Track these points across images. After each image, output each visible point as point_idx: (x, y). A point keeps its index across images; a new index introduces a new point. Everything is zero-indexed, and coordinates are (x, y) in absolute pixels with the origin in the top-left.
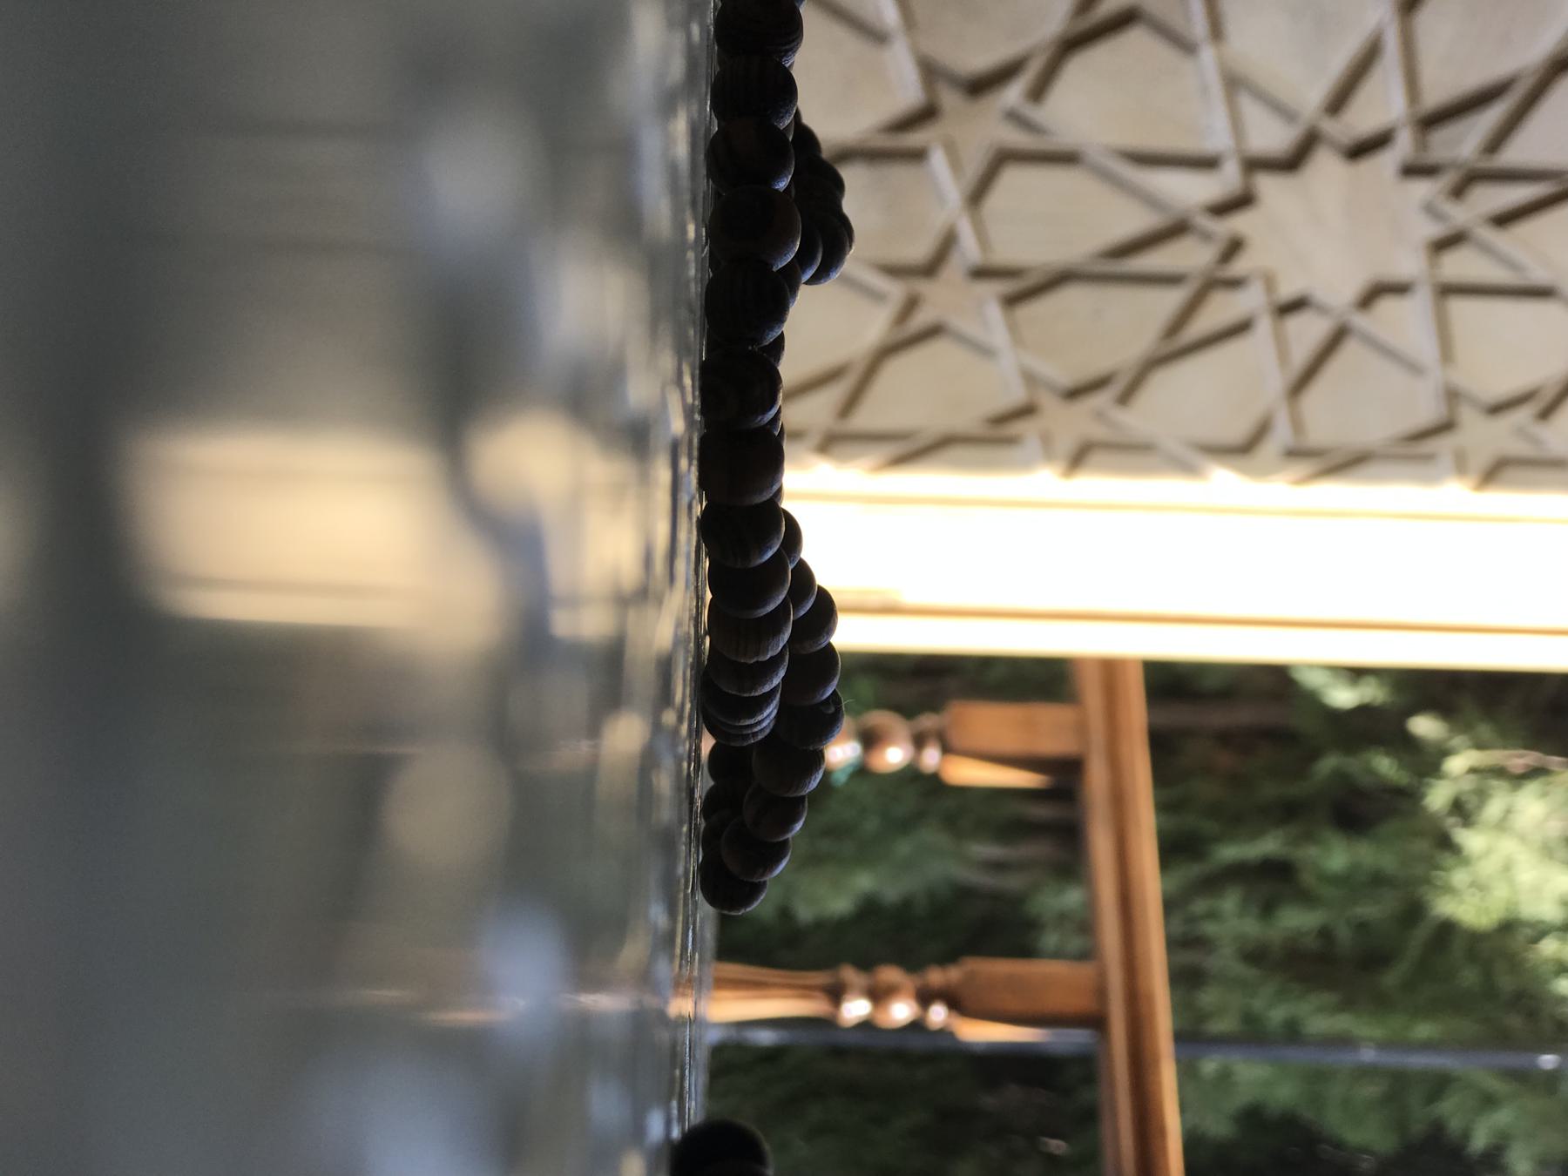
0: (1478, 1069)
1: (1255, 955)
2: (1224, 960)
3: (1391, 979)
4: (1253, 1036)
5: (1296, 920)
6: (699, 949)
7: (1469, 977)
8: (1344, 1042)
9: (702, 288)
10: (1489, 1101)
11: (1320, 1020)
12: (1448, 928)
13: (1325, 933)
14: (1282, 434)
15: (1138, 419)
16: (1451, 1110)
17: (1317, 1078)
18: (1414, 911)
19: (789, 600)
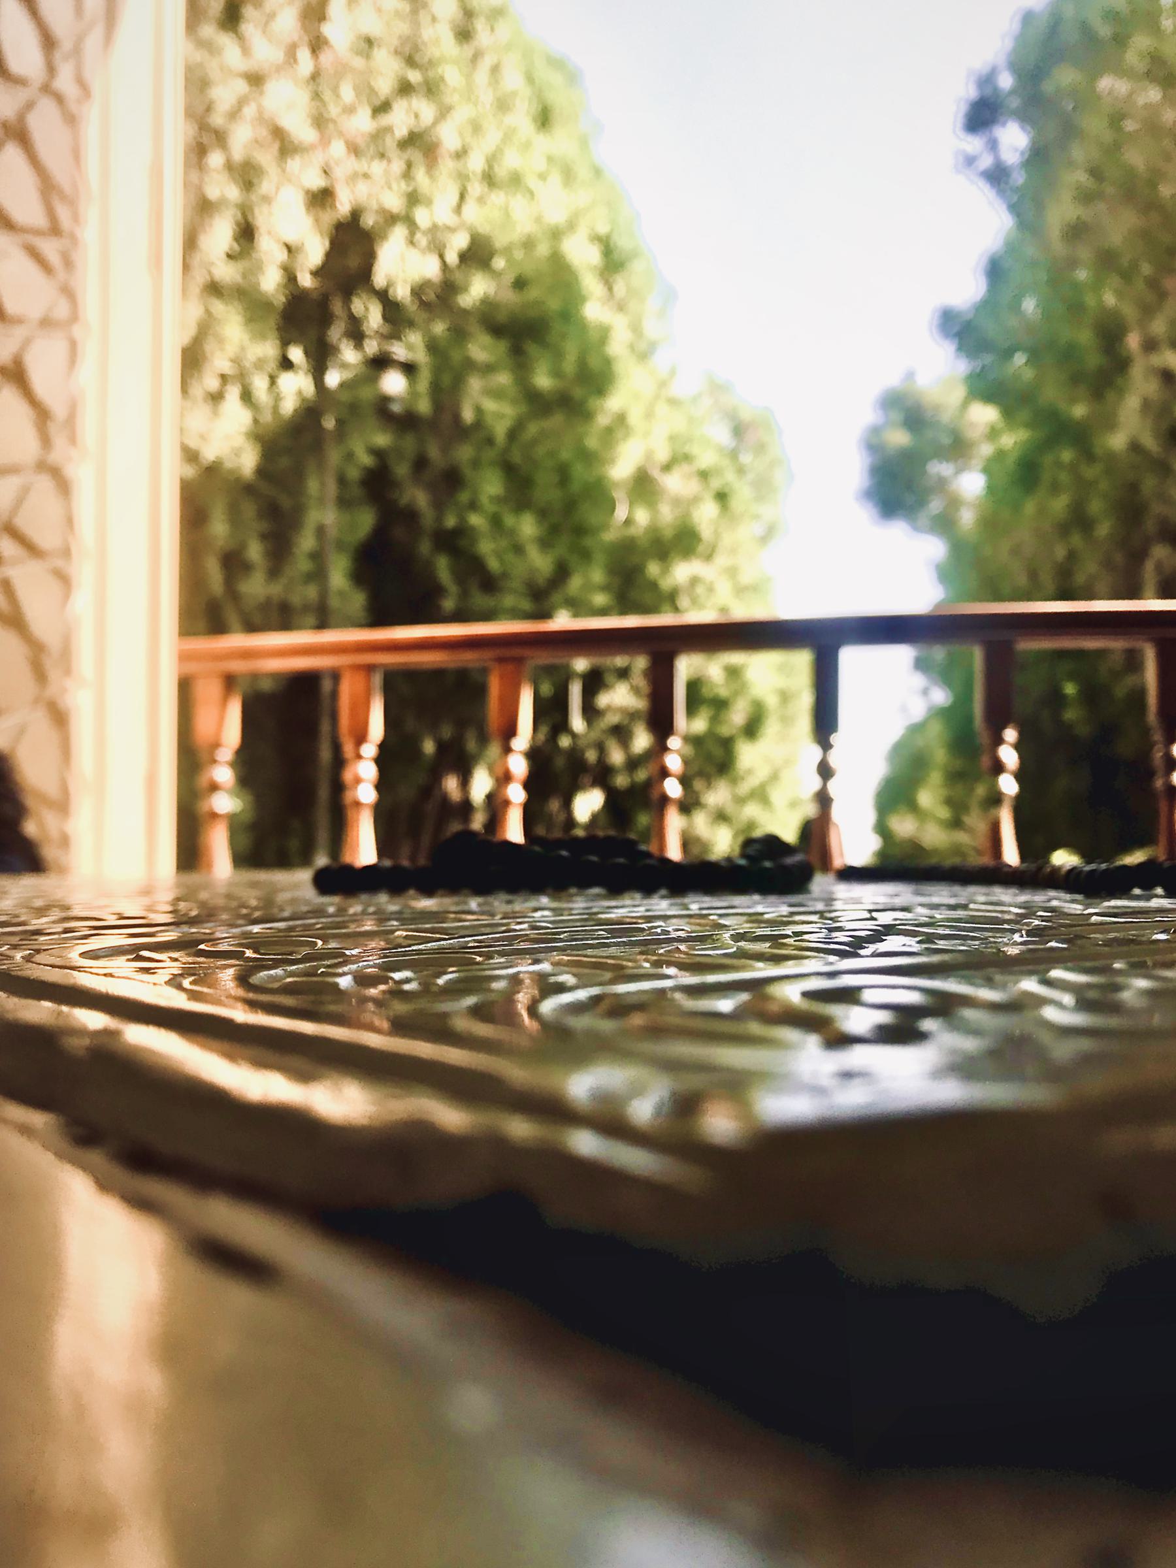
0: (334, 456)
1: (275, 570)
2: (276, 590)
3: (285, 502)
4: (318, 574)
5: (255, 551)
6: (634, 956)
7: (284, 462)
8: (321, 531)
9: (942, 891)
10: (350, 456)
11: (306, 542)
12: (261, 471)
13: (264, 537)
14: (59, 563)
15: (58, 408)
16: (354, 474)
17: (340, 546)
18: (248, 489)
19: (410, 724)
